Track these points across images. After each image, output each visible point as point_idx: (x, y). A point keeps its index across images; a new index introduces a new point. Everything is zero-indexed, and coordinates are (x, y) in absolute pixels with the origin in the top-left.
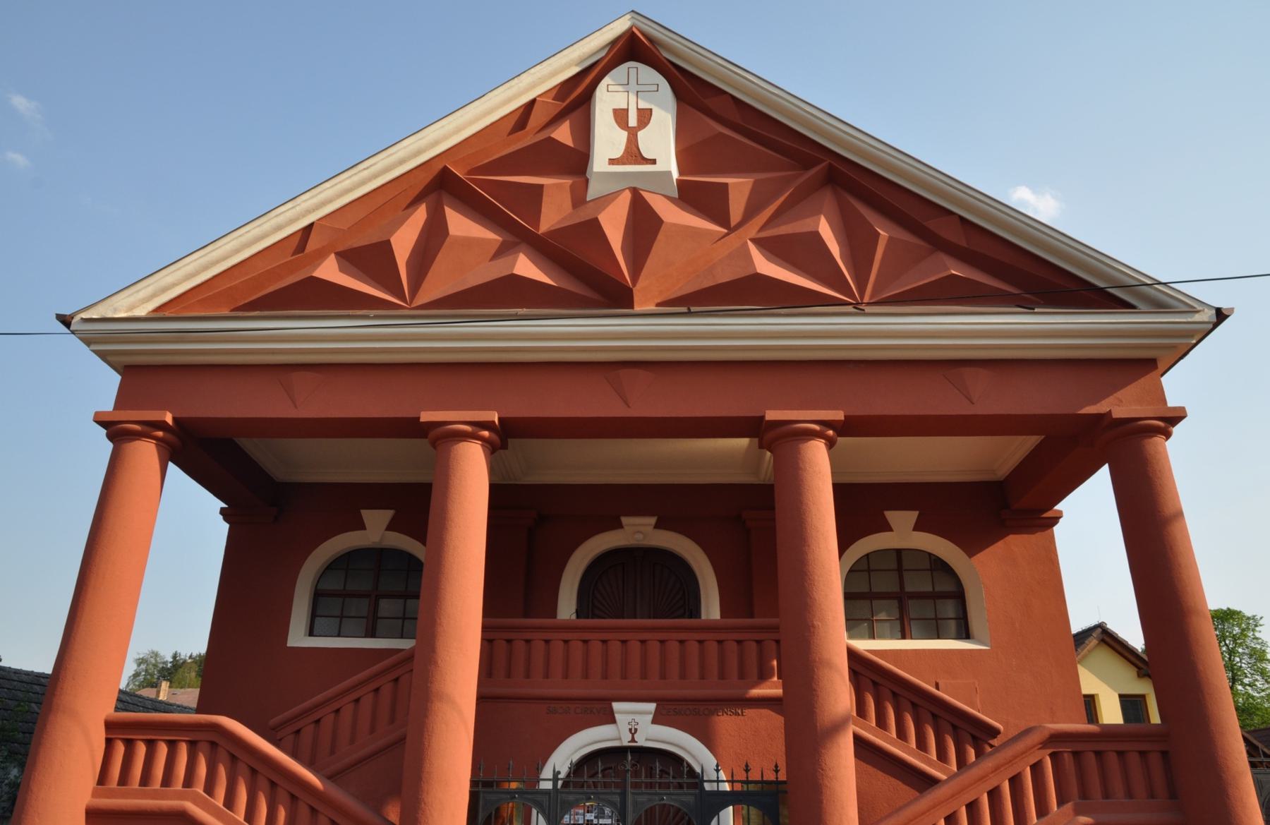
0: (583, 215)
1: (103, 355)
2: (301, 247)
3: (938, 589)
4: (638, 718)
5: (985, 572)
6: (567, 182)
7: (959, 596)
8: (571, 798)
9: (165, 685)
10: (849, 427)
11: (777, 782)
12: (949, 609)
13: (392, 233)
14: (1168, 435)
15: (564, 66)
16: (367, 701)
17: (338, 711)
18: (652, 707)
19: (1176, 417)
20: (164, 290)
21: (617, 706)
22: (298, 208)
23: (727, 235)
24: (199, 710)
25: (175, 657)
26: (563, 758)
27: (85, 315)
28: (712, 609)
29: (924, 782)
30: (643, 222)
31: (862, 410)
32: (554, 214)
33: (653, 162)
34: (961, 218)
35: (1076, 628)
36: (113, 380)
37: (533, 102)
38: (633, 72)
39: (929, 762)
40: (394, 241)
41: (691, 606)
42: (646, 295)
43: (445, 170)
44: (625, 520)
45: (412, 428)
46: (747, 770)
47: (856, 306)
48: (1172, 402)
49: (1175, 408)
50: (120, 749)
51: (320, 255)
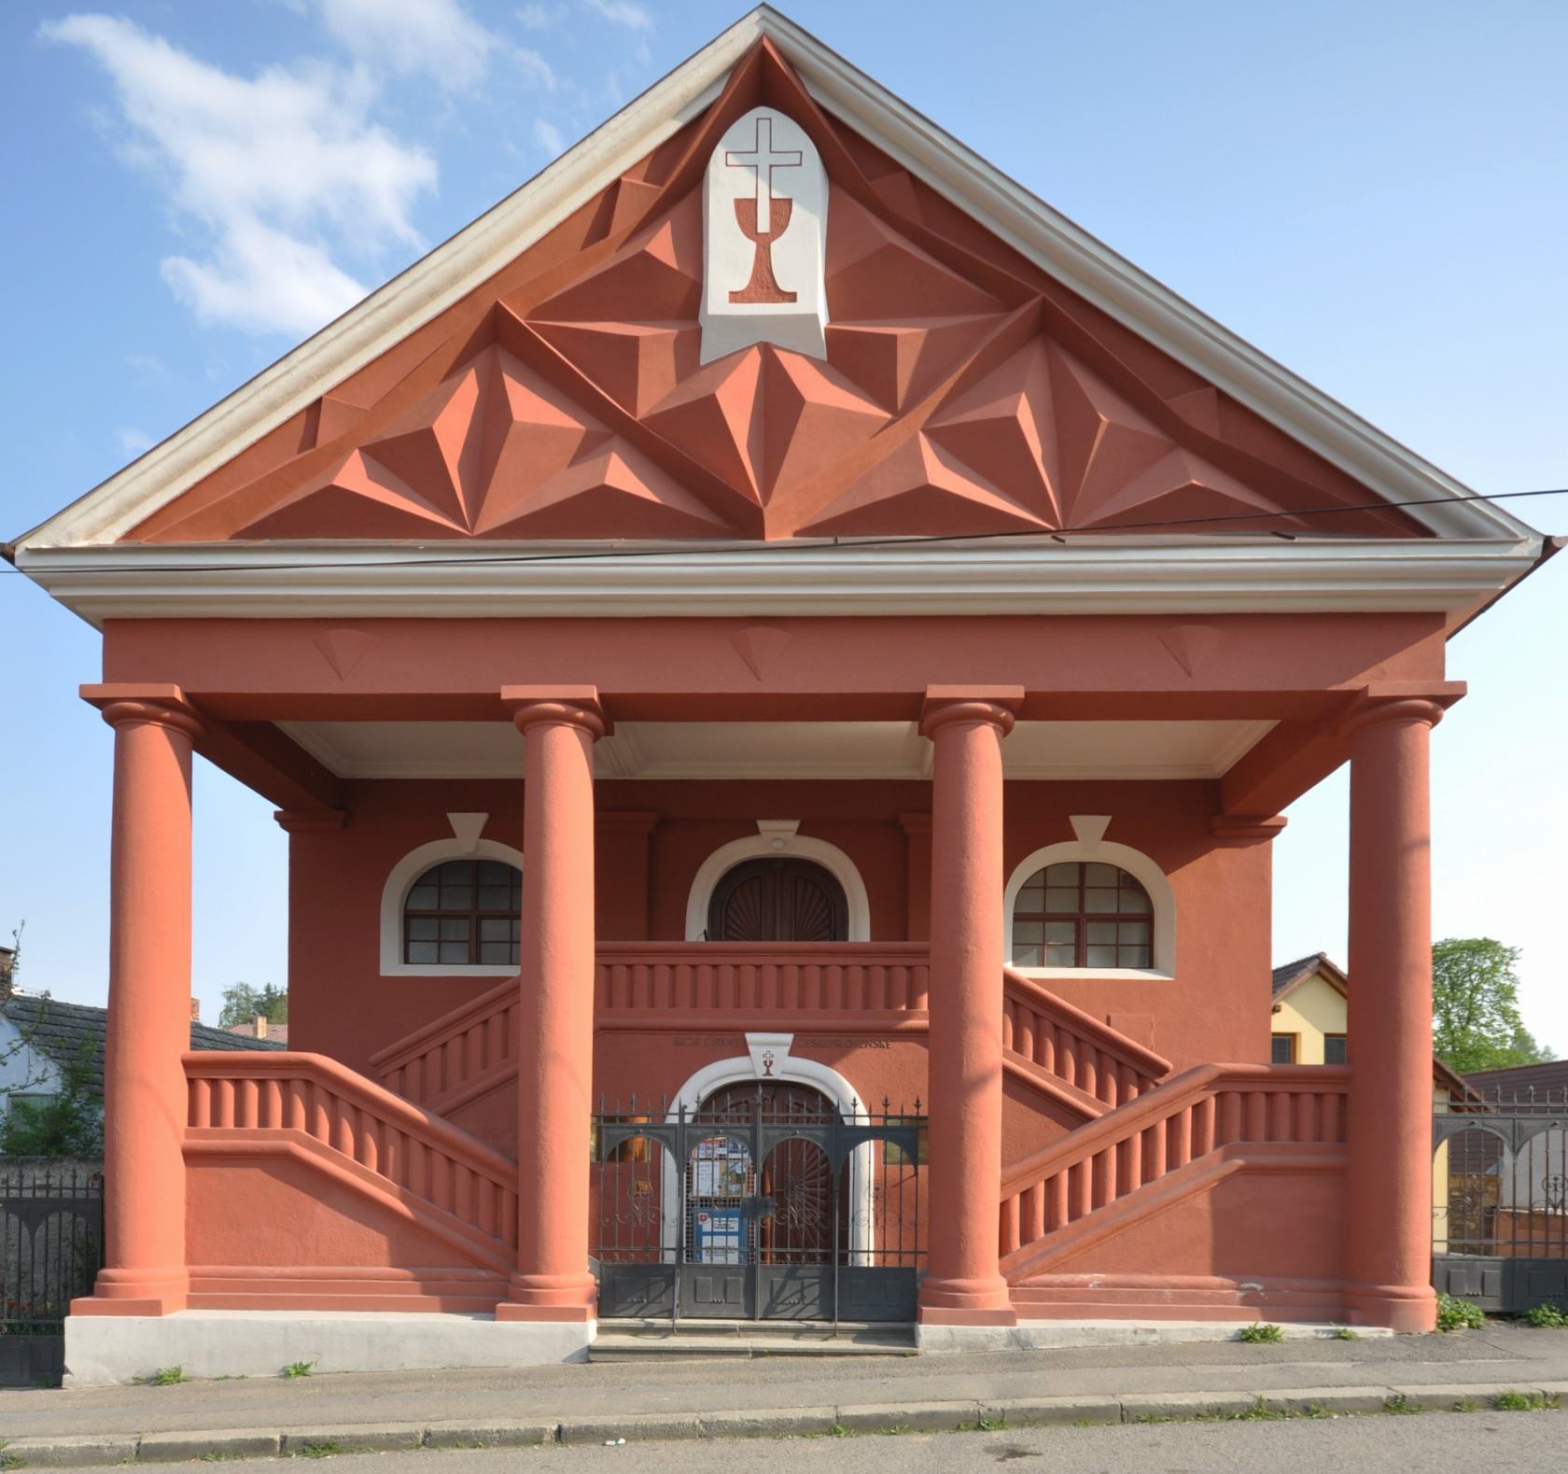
0: (693, 391)
1: (70, 603)
2: (310, 439)
3: (1122, 911)
4: (773, 1050)
5: (1179, 893)
6: (669, 332)
7: (1148, 919)
8: (699, 1132)
9: (261, 1021)
10: (1030, 708)
11: (918, 1118)
12: (1134, 933)
13: (434, 416)
14: (1434, 719)
15: (654, 123)
16: (476, 1034)
17: (444, 1045)
18: (789, 1038)
19: (1449, 697)
20: (133, 504)
21: (750, 1037)
22: (294, 373)
23: (891, 422)
24: (291, 1047)
25: (268, 989)
26: (693, 1092)
27: (31, 544)
28: (860, 929)
29: (1079, 1119)
30: (778, 401)
31: (1045, 685)
32: (655, 391)
33: (792, 297)
34: (1221, 394)
35: (1280, 959)
36: (93, 640)
37: (617, 184)
38: (764, 125)
39: (1087, 1100)
40: (438, 428)
41: (836, 924)
42: (783, 513)
43: (497, 311)
44: (762, 824)
45: (491, 708)
46: (886, 1105)
47: (1055, 534)
48: (1451, 675)
49: (1453, 684)
50: (205, 1090)
51: (338, 453)
